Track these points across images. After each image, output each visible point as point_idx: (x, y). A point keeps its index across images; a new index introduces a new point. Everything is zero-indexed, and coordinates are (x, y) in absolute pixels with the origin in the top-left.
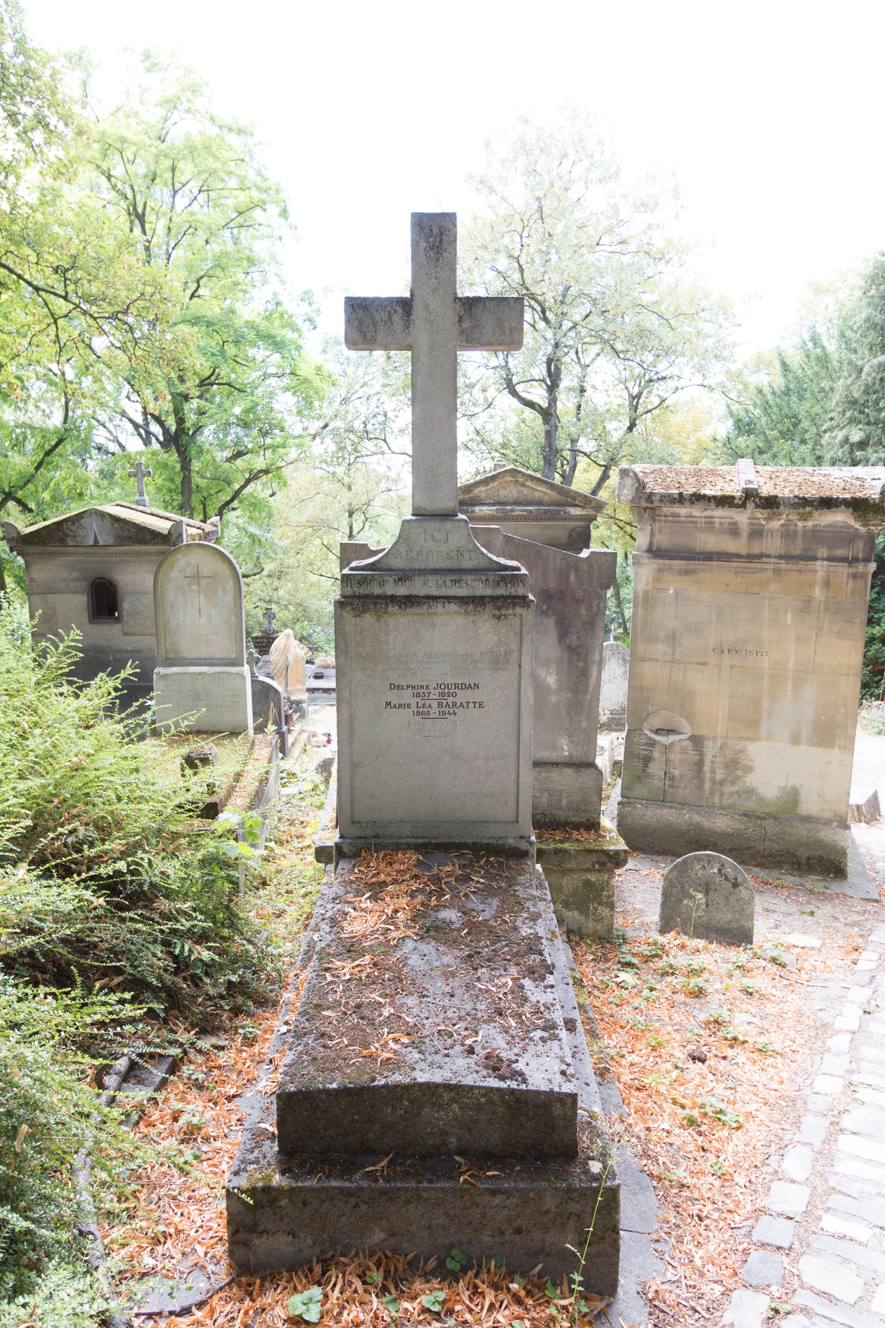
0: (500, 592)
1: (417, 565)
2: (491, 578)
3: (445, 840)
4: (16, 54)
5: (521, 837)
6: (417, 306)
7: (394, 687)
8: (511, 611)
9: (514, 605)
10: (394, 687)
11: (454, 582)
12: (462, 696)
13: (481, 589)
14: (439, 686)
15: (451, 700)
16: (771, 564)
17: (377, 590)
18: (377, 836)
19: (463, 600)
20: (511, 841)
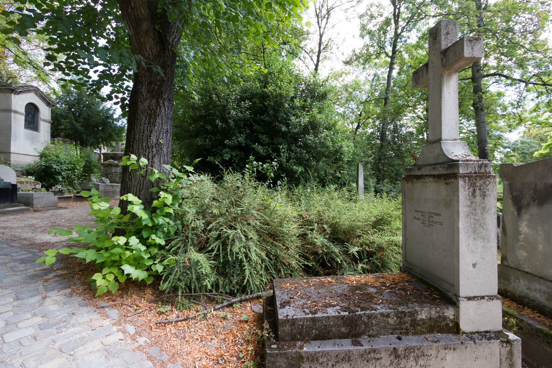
0: (449, 172)
1: (425, 163)
2: (445, 166)
3: (428, 281)
4: (422, 48)
5: (455, 295)
6: (430, 65)
7: (417, 211)
8: (450, 181)
9: (451, 178)
10: (417, 211)
11: (434, 168)
12: (436, 218)
13: (442, 171)
14: (428, 212)
15: (432, 219)
16: (72, 199)
17: (413, 173)
18: (411, 269)
19: (434, 176)
20: (450, 294)
